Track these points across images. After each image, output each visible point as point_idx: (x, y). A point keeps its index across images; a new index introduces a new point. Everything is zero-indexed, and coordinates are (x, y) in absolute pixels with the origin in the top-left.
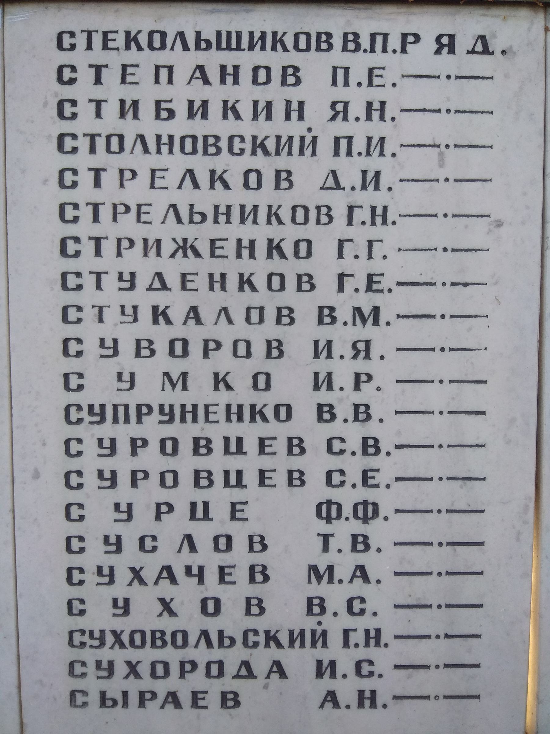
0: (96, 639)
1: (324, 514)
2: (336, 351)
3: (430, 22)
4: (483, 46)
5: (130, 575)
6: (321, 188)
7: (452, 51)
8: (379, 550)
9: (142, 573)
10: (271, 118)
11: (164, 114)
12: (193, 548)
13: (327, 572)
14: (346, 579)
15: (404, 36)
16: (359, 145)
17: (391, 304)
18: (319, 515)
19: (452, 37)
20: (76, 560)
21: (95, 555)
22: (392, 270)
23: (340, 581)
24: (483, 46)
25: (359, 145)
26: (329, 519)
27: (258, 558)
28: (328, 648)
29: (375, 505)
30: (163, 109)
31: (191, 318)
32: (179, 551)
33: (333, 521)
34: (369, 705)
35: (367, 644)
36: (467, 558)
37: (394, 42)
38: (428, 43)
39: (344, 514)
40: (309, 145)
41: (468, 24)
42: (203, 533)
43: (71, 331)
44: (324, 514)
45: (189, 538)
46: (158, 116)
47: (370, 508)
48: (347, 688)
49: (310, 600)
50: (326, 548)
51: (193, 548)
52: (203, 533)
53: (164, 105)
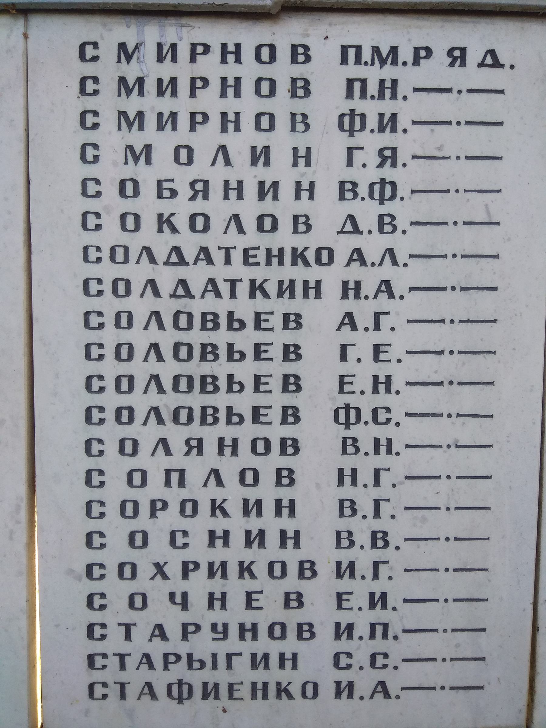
0: (220, 633)
1: (347, 126)
2: (361, 479)
3: (441, 35)
4: (491, 59)
5: (154, 570)
6: (338, 233)
7: (463, 64)
8: (394, 609)
9: (165, 569)
10: (284, 667)
11: (166, 194)
12: (220, 483)
13: (341, 632)
14: (371, 295)
15: (417, 50)
16: (373, 88)
17: (404, 177)
18: (341, 127)
19: (463, 50)
20: (98, 647)
21: (116, 551)
22: (397, 588)
23: (366, 297)
24: (491, 59)
25: (373, 88)
26: (351, 132)
27: (291, 368)
28: (357, 486)
29: (393, 185)
30: (165, 189)
31: (210, 291)
32: (213, 164)
33: (356, 133)
34: (390, 96)
35: (377, 451)
36: (476, 462)
37: (406, 54)
38: (440, 55)
39: (369, 126)
40: (325, 256)
41: (476, 37)
42: (230, 468)
43: (89, 69)
44: (347, 126)
45: (216, 472)
46: (160, 196)
47: (388, 188)
48: (365, 680)
49: (341, 503)
50: (344, 357)
51: (220, 483)
52: (230, 468)
53: (165, 185)
